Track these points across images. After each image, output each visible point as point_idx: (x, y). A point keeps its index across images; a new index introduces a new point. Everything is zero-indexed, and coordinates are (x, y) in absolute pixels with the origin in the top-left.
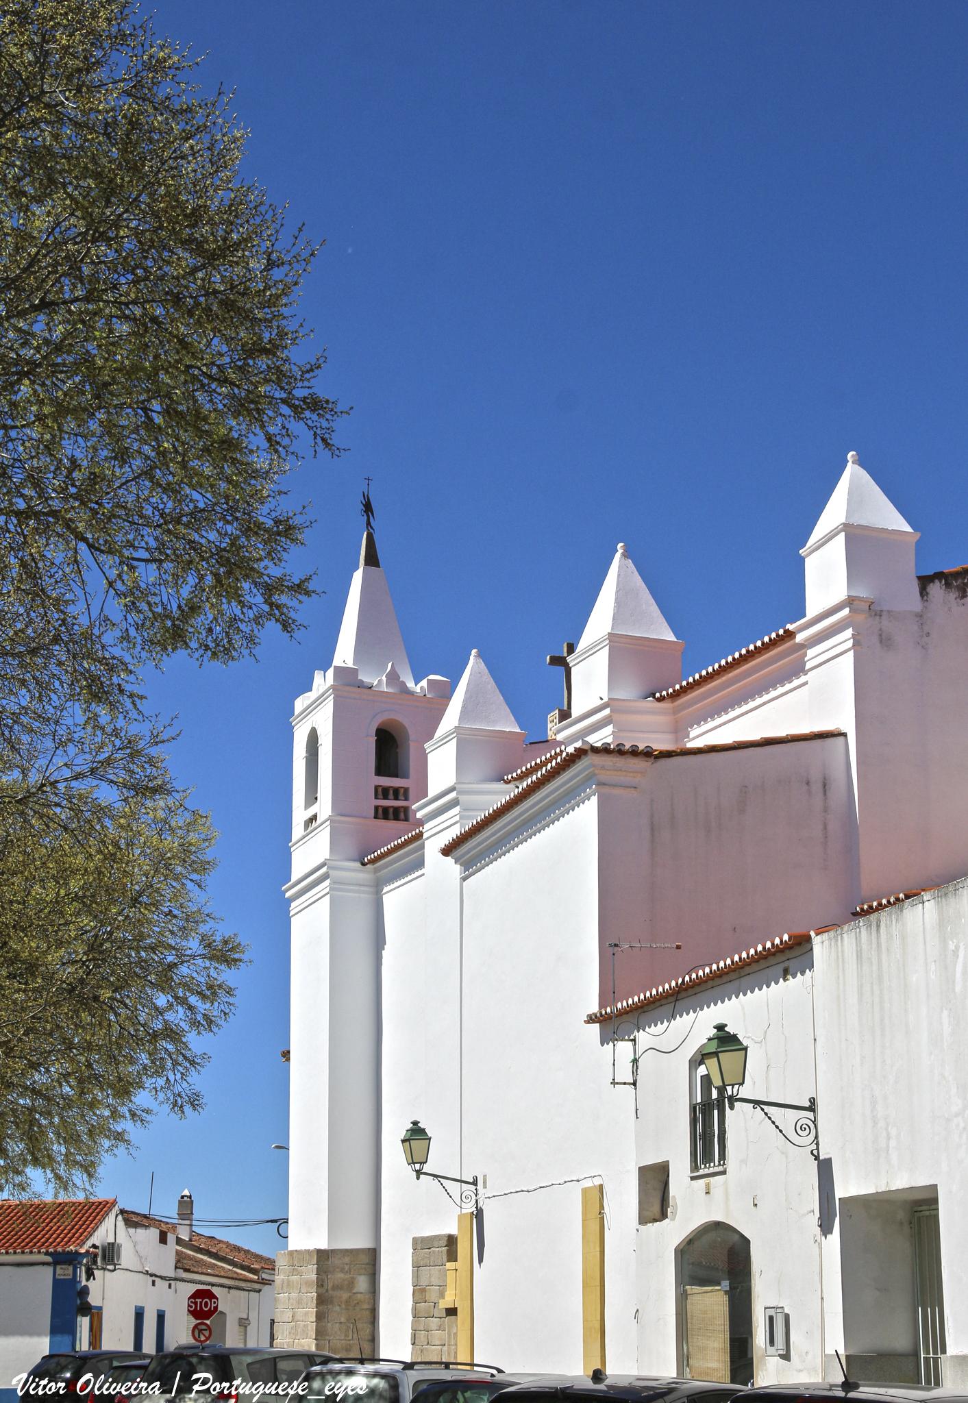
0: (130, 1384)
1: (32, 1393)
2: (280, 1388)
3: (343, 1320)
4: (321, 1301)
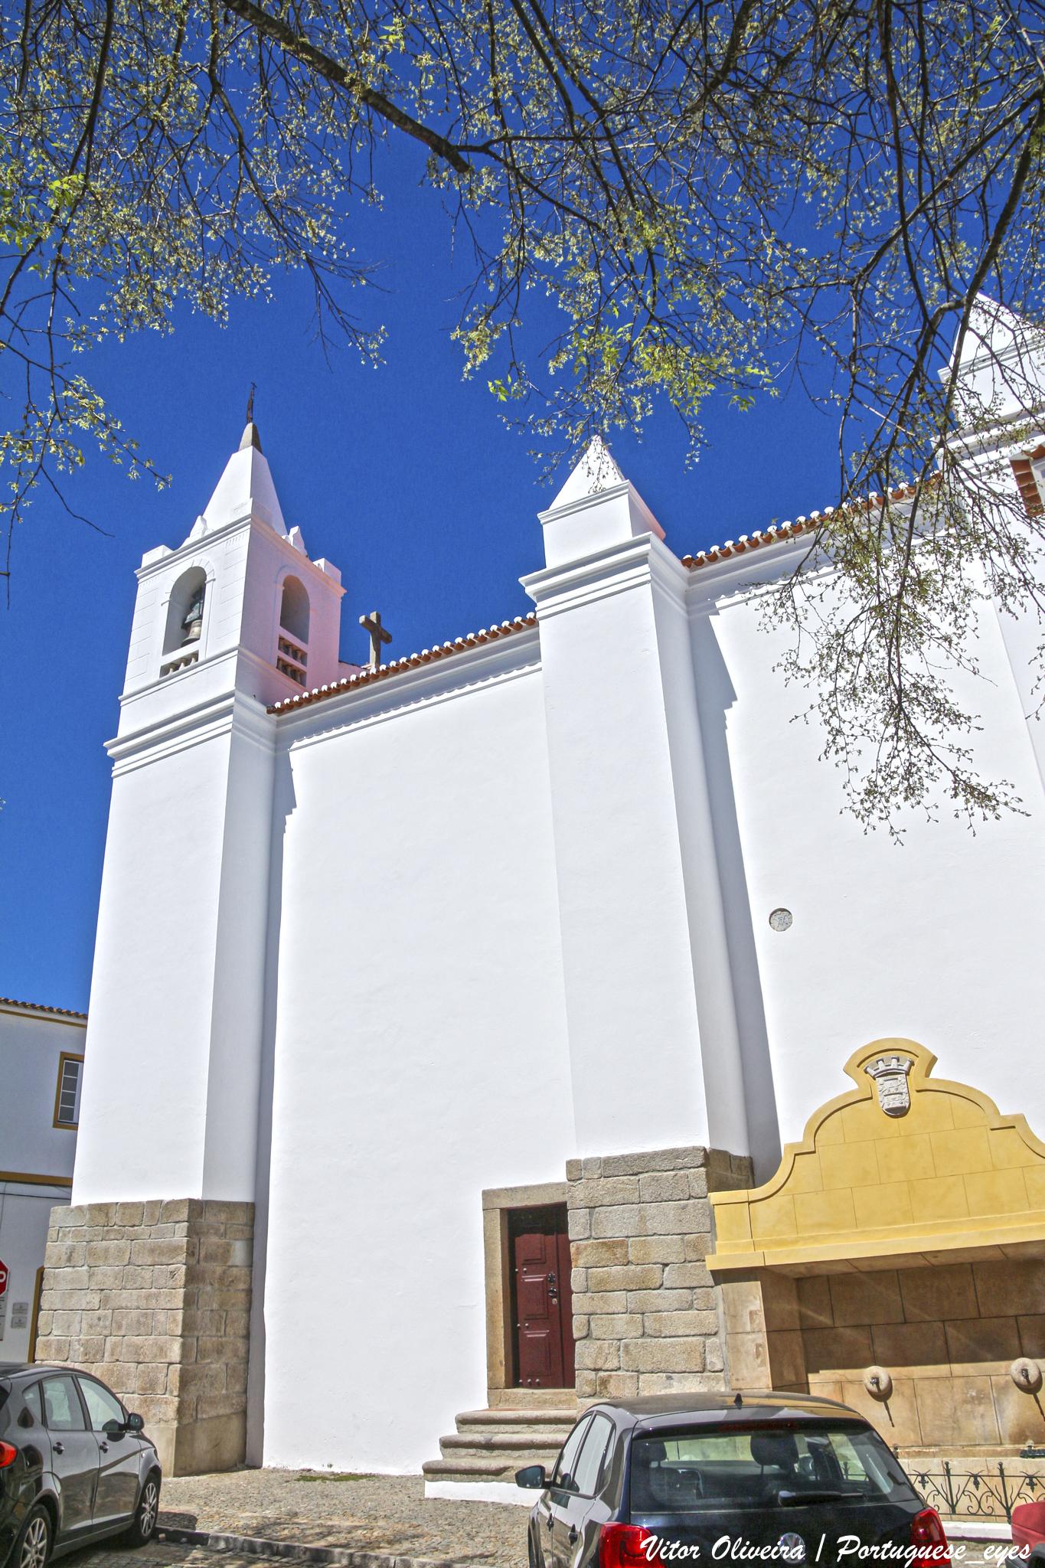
0: (769, 1547)
1: (663, 1557)
2: (935, 1552)
3: (215, 1306)
4: (193, 1277)
